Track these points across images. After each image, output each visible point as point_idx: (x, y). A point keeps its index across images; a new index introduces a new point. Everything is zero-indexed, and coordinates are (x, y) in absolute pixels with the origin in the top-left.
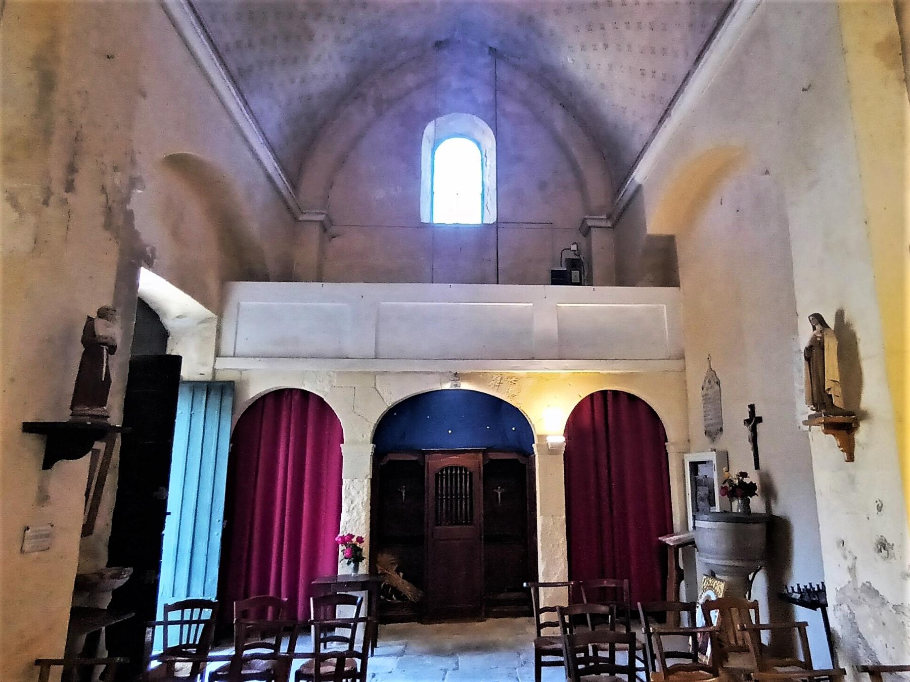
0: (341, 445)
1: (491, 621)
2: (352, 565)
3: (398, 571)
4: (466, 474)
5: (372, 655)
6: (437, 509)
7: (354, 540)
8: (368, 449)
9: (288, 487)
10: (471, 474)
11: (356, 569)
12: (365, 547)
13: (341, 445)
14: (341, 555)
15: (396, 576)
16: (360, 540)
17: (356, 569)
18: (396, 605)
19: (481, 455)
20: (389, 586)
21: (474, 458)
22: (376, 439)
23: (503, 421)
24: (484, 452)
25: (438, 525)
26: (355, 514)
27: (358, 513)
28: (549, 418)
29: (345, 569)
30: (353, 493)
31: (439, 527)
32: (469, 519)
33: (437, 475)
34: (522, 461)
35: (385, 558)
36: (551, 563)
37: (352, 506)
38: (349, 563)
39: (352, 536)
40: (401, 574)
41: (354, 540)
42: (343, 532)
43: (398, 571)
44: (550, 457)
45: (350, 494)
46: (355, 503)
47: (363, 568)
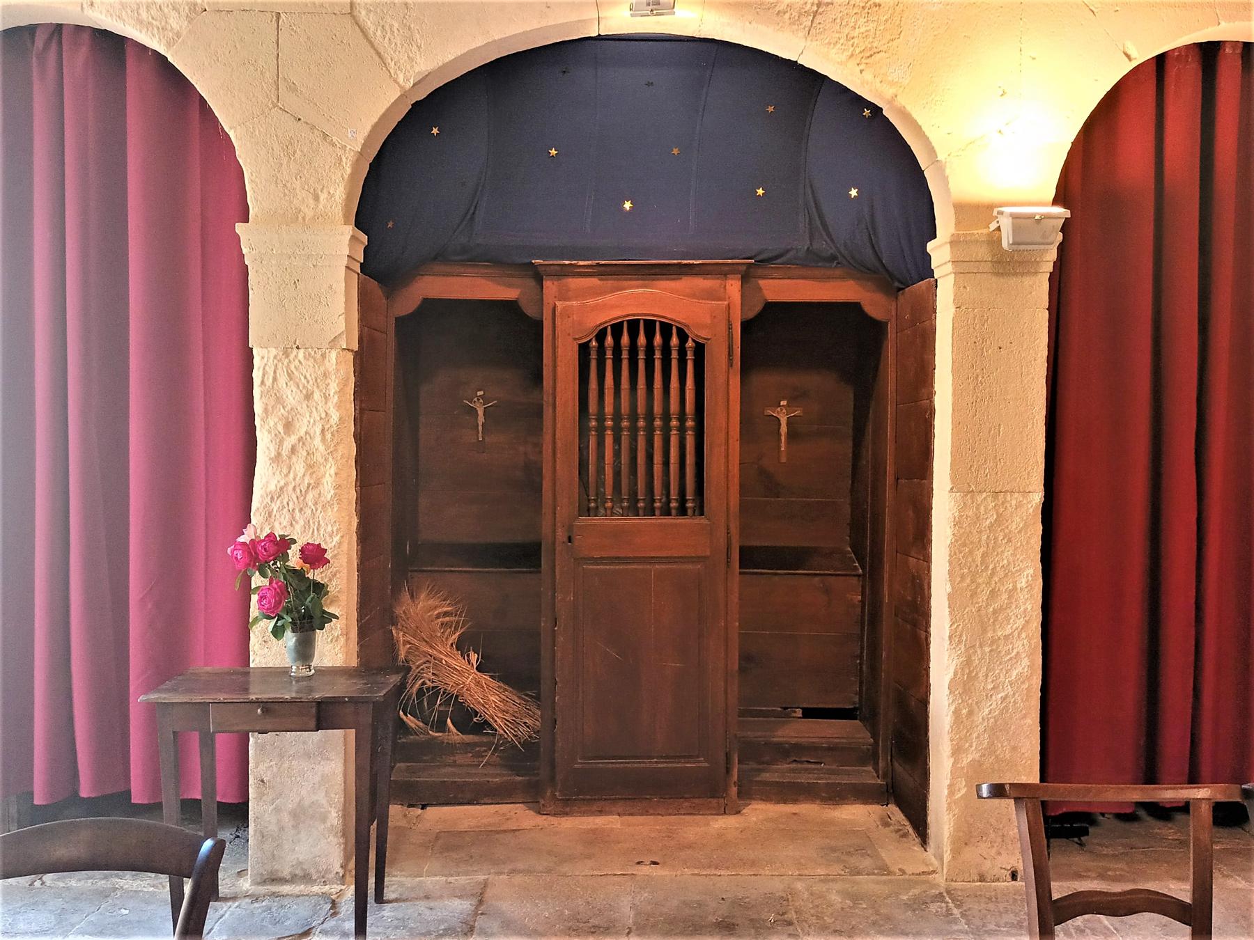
0: (240, 228)
1: (759, 813)
2: (290, 638)
3: (461, 646)
4: (682, 352)
5: (379, 898)
6: (583, 450)
7: (294, 559)
8: (341, 243)
9: (201, 426)
10: (700, 349)
11: (304, 651)
12: (341, 581)
13: (240, 228)
14: (254, 611)
15: (457, 662)
16: (314, 555)
17: (304, 651)
18: (451, 748)
19: (733, 287)
20: (436, 692)
21: (710, 295)
22: (368, 212)
23: (826, 143)
24: (746, 277)
25: (588, 512)
26: (300, 467)
27: (311, 467)
28: (998, 137)
29: (270, 650)
30: (292, 397)
31: (596, 521)
32: (692, 499)
33: (584, 349)
34: (874, 304)
35: (427, 613)
36: (979, 633)
37: (289, 442)
38: (277, 632)
39: (284, 544)
40: (474, 657)
41: (294, 559)
42: (258, 528)
43: (461, 646)
44: (994, 279)
45: (279, 400)
46: (301, 428)
47: (335, 648)
